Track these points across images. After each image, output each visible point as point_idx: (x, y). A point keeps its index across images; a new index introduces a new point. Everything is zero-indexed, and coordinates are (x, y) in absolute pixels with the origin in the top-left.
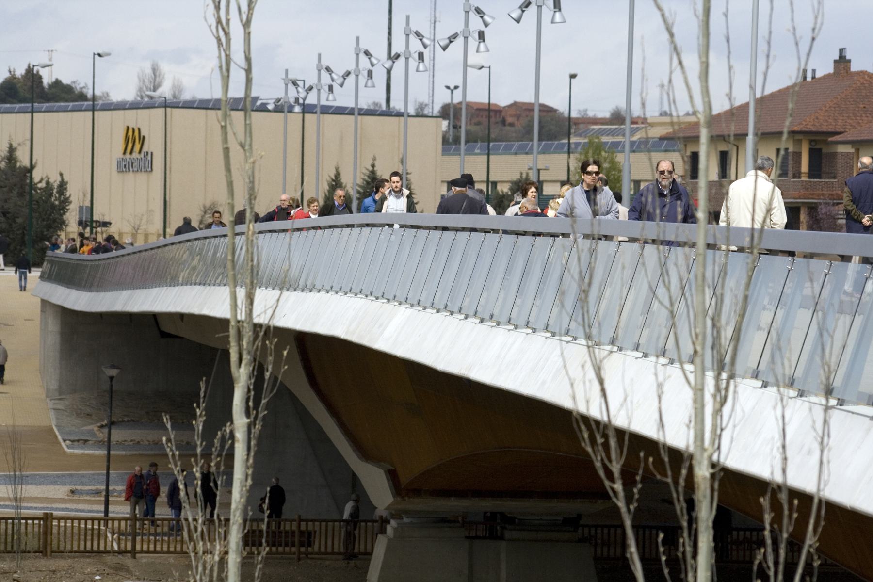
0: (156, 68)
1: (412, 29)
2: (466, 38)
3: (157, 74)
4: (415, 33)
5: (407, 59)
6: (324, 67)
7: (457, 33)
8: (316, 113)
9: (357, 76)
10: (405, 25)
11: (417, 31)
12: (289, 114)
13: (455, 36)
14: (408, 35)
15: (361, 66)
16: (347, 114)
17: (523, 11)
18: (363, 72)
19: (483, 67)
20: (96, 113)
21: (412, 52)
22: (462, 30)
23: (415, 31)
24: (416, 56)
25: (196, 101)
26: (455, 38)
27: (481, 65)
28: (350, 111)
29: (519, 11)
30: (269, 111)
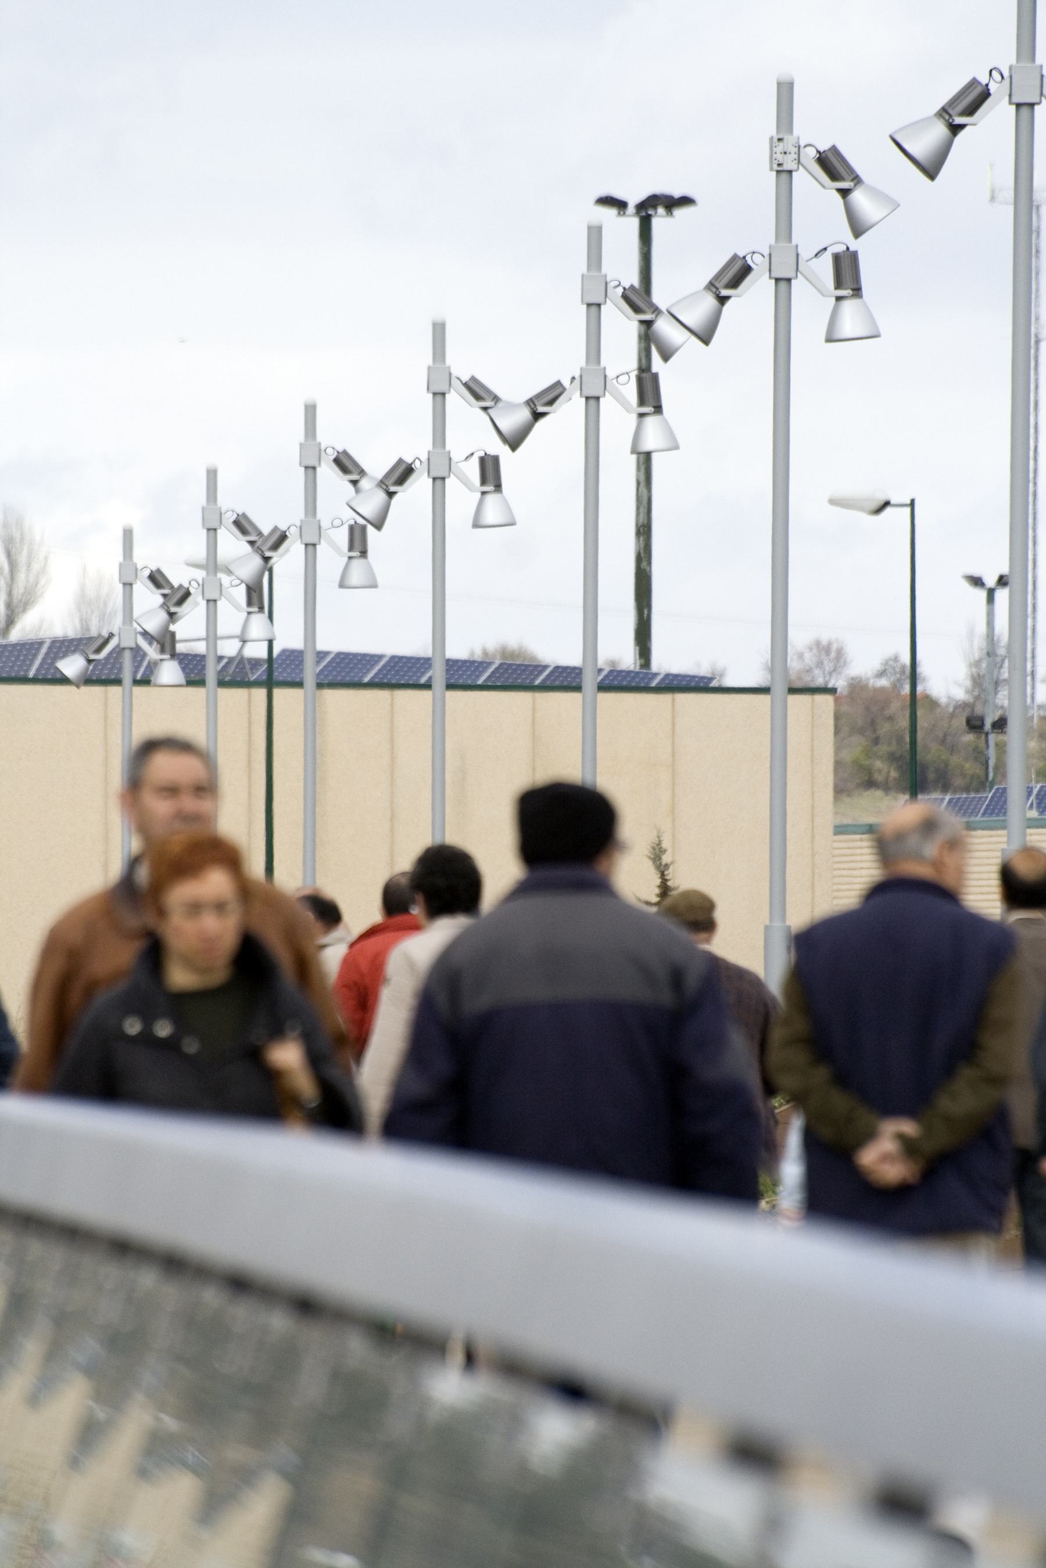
0: (17, 536)
1: (455, 372)
2: (592, 400)
3: (22, 559)
4: (466, 385)
5: (439, 481)
6: (230, 518)
7: (558, 384)
8: (427, 686)
9: (311, 547)
10: (429, 361)
11: (473, 379)
12: (138, 690)
13: (553, 395)
14: (440, 396)
15: (324, 514)
16: (372, 685)
17: (723, 300)
18: (332, 533)
19: (887, 504)
20: (277, 692)
21: (455, 457)
22: (577, 375)
23: (465, 378)
24: (473, 470)
25: (41, 643)
26: (551, 403)
27: (882, 498)
28: (663, 680)
29: (709, 302)
30: (64, 680)
